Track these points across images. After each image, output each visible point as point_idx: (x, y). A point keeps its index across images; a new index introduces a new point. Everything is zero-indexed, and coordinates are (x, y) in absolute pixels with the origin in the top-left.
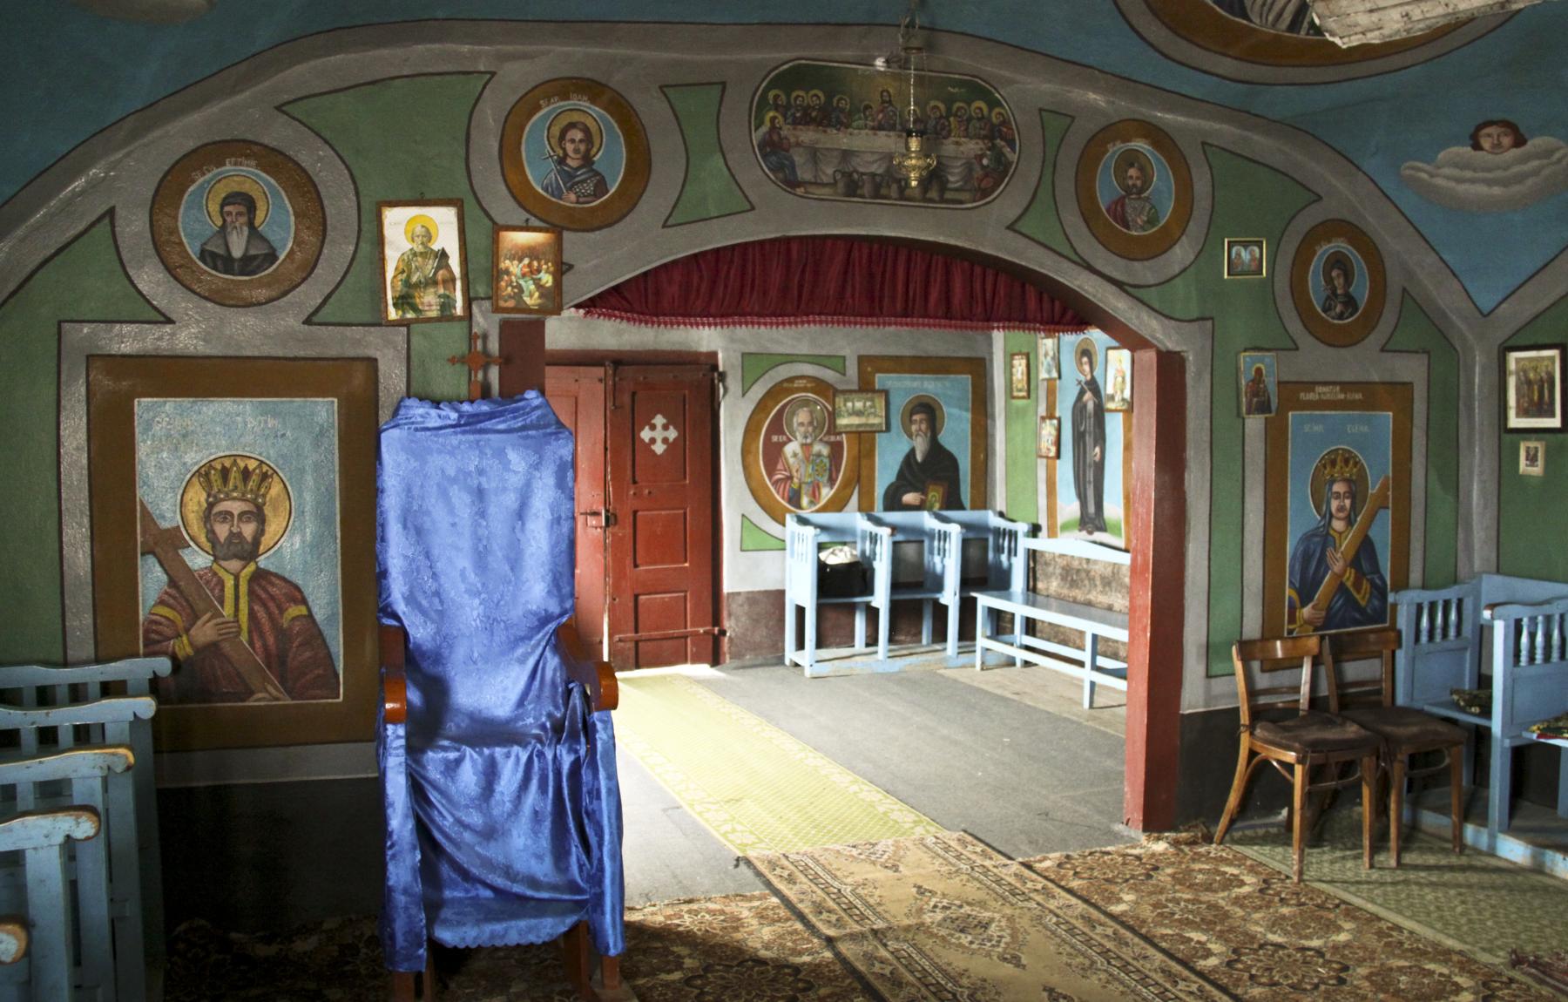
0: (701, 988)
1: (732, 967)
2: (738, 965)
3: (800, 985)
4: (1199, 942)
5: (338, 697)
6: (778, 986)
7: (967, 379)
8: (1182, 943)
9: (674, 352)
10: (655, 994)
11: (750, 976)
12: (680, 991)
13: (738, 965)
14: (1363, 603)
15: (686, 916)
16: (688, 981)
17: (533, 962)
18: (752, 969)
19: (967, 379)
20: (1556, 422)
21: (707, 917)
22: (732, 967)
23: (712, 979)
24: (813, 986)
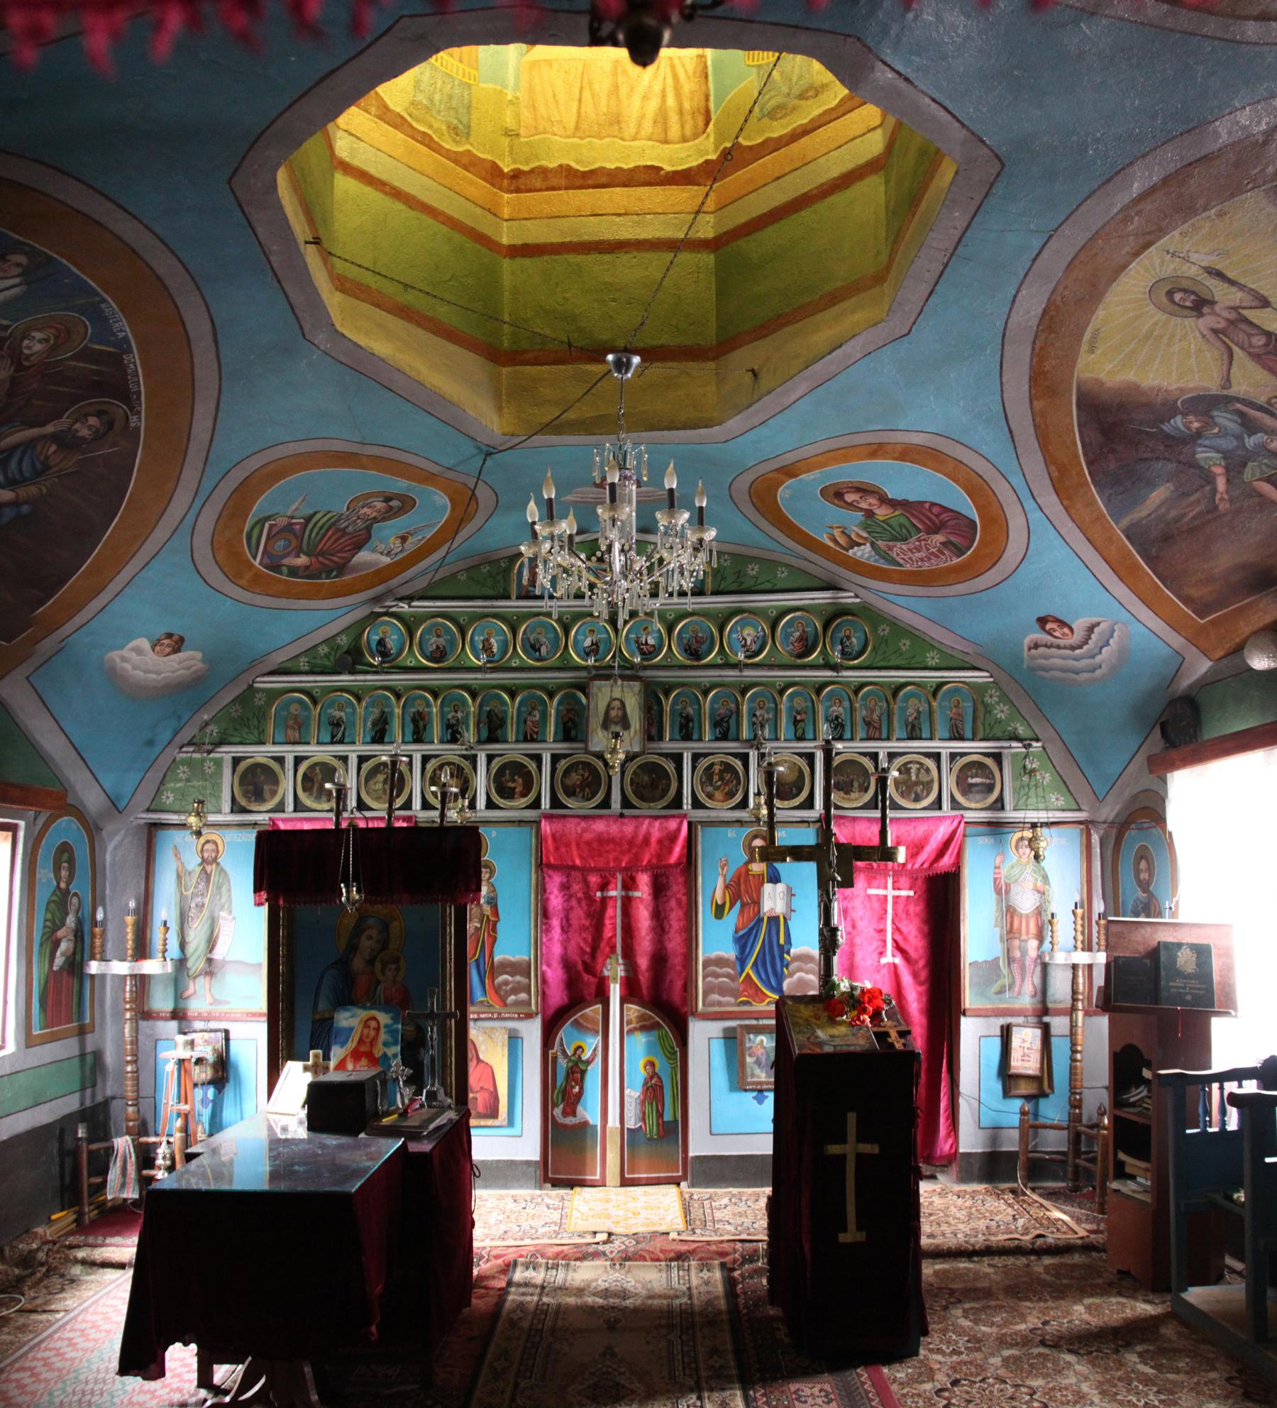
0: (948, 1399)
1: (975, 1382)
2: (980, 1382)
3: (946, 1394)
4: (1146, 1364)
5: (595, 1175)
6: (967, 1397)
7: (10, 834)
8: (1161, 1365)
9: (962, 917)
10: (909, 1401)
11: (991, 1392)
12: (930, 1399)
13: (980, 1382)
14: (569, 1054)
15: (963, 1349)
16: (939, 1392)
17: (991, 1380)
18: (993, 1385)
19: (10, 834)
20: (22, 824)
21: (944, 1347)
22: (975, 1382)
23: (958, 1393)
24: (936, 1393)
